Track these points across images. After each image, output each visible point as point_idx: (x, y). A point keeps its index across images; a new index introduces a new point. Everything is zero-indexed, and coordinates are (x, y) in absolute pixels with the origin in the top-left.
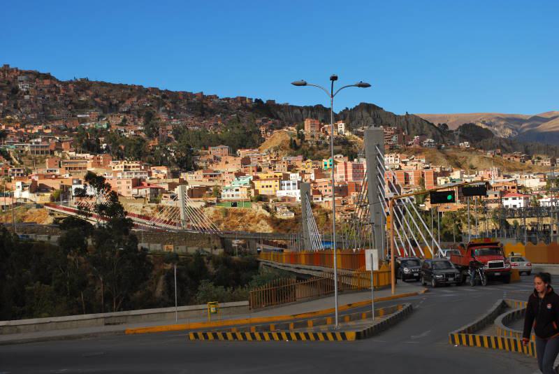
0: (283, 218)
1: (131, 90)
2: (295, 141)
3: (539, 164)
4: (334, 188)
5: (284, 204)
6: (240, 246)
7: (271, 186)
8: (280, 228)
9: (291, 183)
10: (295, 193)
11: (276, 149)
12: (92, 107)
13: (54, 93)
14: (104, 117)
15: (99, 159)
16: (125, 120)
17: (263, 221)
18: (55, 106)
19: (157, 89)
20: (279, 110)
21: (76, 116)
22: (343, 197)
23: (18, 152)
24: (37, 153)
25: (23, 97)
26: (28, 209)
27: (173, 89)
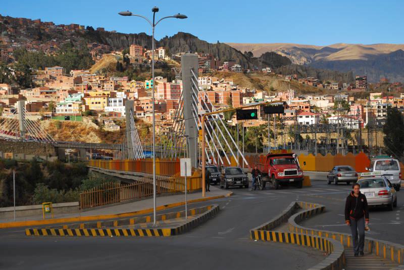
0: (110, 130)
5: (111, 118)
6: (72, 155)
7: (99, 103)
11: (104, 71)
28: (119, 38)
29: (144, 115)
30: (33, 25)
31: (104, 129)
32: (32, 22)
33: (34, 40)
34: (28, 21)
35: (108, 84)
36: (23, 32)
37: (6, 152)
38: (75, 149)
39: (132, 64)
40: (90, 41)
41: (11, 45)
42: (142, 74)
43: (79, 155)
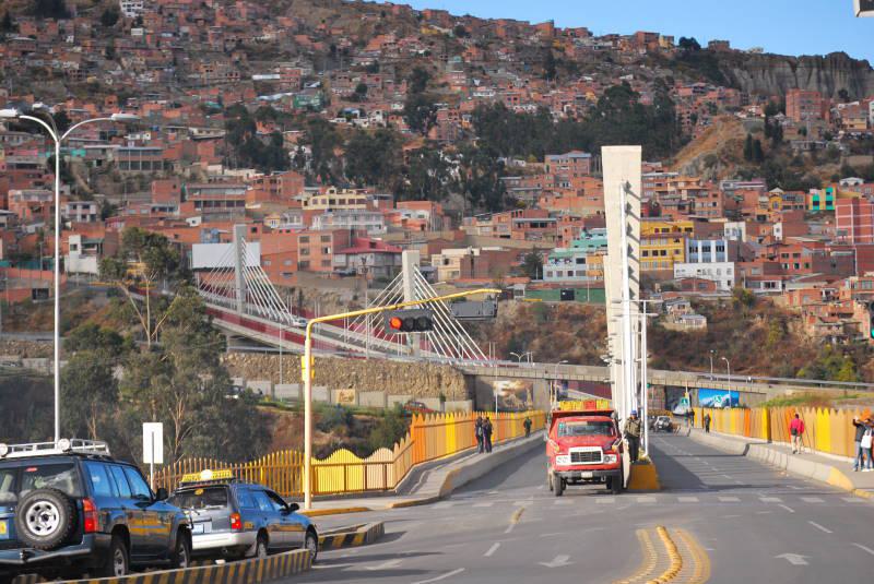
0: (678, 329)
1: (383, 15)
2: (758, 143)
6: (513, 396)
7: (664, 253)
8: (669, 354)
9: (300, 245)
10: (719, 272)
11: (711, 162)
12: (288, 56)
13: (201, 23)
14: (315, 80)
16: (362, 89)
18: (203, 53)
19: (444, 13)
20: (740, 65)
21: (250, 78)
22: (830, 282)
23: (89, 164)
24: (134, 165)
25: (128, 32)
26: (88, 298)
27: (483, 13)
28: (772, 67)
29: (784, 286)
30: (532, 38)
31: (664, 324)
32: (532, 29)
33: (533, 80)
34: (520, 28)
35: (704, 200)
36: (504, 58)
37: (338, 387)
38: (518, 382)
39: (789, 142)
40: (688, 78)
41: (471, 94)
42: (816, 170)
43: (529, 396)
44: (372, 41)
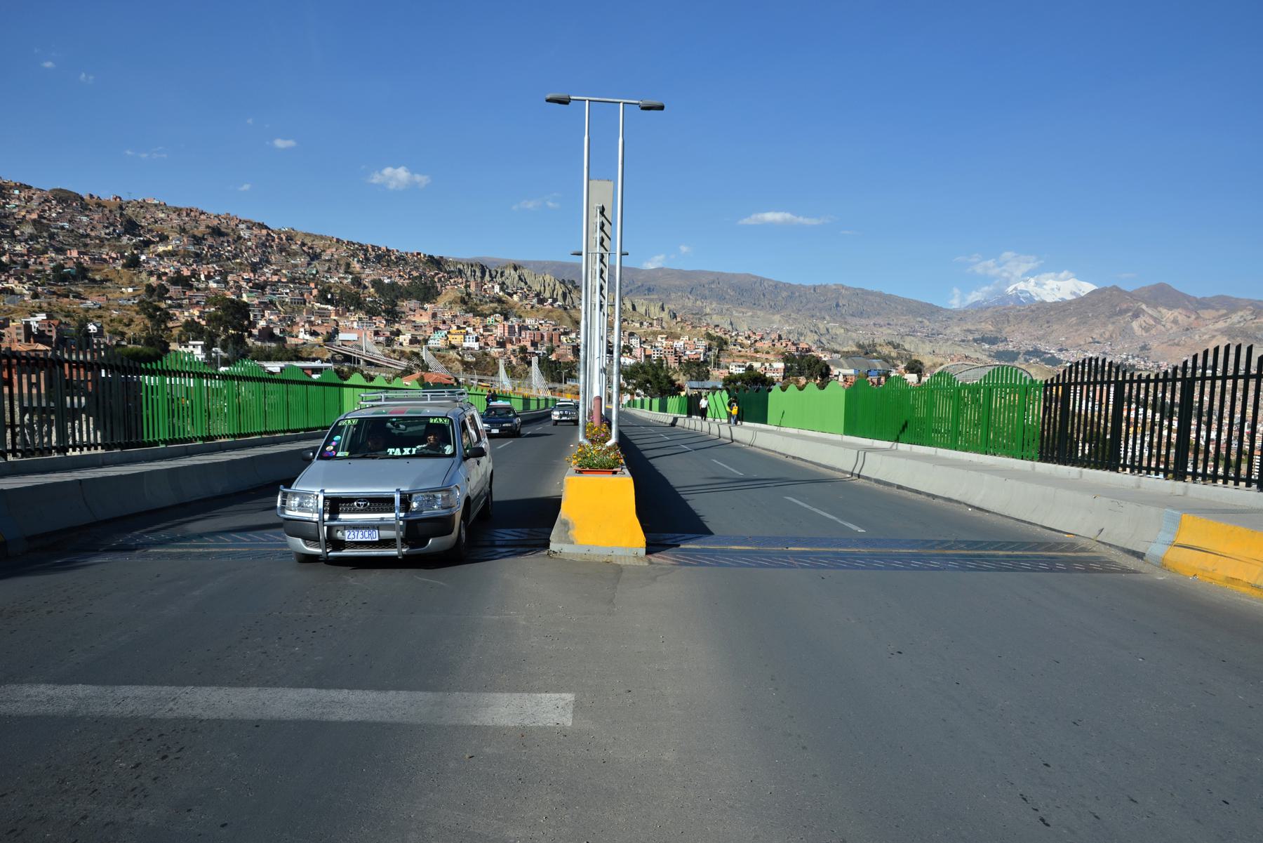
3: (632, 325)
4: (497, 342)
11: (450, 303)
15: (339, 310)
17: (457, 362)
44: (328, 250)
